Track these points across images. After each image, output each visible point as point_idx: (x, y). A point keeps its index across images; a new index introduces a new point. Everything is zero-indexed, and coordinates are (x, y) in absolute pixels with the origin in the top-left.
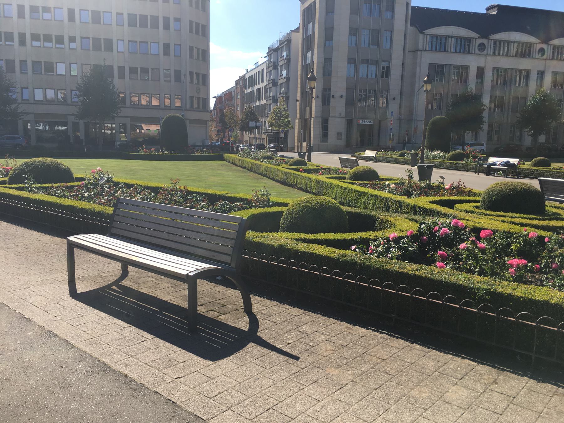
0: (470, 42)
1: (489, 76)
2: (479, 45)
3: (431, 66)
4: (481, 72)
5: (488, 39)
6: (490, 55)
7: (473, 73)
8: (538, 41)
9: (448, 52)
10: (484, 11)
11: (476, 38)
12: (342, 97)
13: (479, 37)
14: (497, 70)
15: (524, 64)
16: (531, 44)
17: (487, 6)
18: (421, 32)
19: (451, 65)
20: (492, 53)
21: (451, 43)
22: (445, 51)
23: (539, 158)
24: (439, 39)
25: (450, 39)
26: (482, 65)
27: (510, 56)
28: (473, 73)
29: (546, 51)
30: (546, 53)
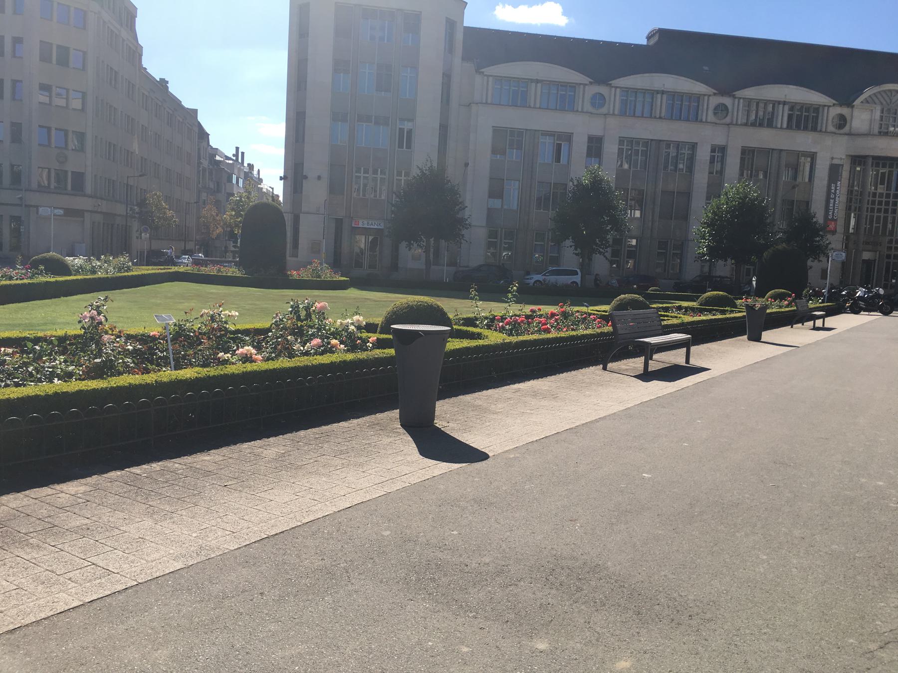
0: (818, 113)
1: (611, 149)
2: (594, 97)
3: (498, 131)
4: (595, 146)
5: (734, 97)
6: (614, 114)
7: (703, 154)
8: (586, 80)
9: (701, 121)
10: (644, 42)
11: (829, 106)
12: (319, 178)
13: (591, 83)
14: (747, 153)
15: (802, 141)
16: (817, 109)
17: (646, 35)
18: (478, 71)
19: (781, 150)
20: (785, 126)
21: (662, 104)
22: (651, 117)
23: (623, 296)
24: (762, 105)
25: (659, 96)
26: (597, 132)
27: (655, 117)
28: (703, 154)
29: (730, 110)
30: (730, 114)
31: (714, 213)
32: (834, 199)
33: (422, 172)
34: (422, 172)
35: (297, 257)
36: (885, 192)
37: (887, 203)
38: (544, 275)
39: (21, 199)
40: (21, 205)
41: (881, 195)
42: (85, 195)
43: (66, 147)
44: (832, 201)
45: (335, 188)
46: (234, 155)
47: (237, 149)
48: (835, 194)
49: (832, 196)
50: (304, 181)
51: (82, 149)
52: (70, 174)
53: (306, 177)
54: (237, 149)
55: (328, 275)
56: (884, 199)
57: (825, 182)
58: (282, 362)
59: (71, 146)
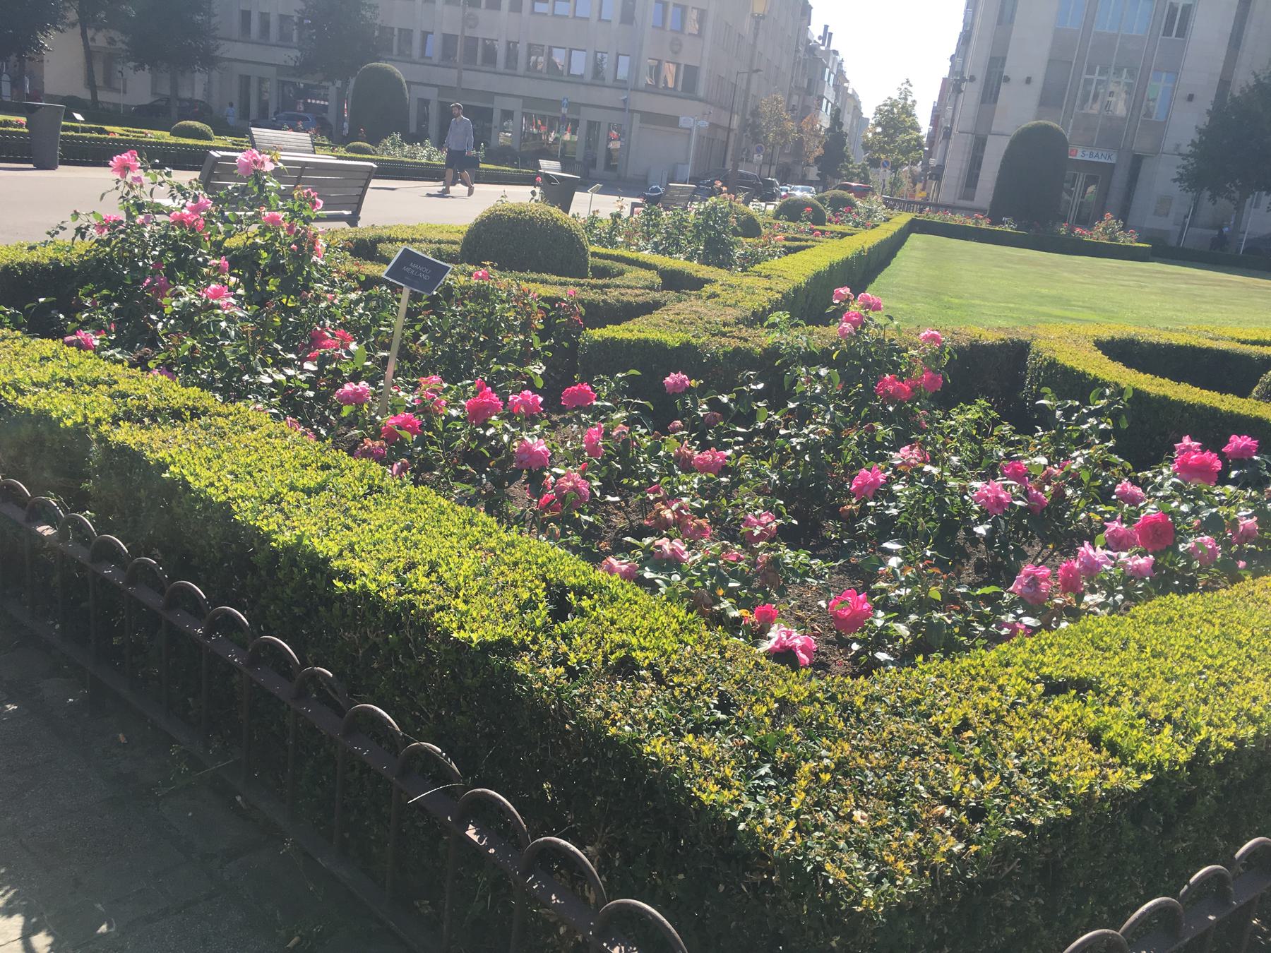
12: (1028, 81)
35: (973, 200)
39: (625, 101)
40: (623, 110)
45: (1050, 98)
46: (820, 38)
47: (826, 27)
52: (682, 68)
53: (1007, 79)
54: (826, 27)
55: (1126, 240)
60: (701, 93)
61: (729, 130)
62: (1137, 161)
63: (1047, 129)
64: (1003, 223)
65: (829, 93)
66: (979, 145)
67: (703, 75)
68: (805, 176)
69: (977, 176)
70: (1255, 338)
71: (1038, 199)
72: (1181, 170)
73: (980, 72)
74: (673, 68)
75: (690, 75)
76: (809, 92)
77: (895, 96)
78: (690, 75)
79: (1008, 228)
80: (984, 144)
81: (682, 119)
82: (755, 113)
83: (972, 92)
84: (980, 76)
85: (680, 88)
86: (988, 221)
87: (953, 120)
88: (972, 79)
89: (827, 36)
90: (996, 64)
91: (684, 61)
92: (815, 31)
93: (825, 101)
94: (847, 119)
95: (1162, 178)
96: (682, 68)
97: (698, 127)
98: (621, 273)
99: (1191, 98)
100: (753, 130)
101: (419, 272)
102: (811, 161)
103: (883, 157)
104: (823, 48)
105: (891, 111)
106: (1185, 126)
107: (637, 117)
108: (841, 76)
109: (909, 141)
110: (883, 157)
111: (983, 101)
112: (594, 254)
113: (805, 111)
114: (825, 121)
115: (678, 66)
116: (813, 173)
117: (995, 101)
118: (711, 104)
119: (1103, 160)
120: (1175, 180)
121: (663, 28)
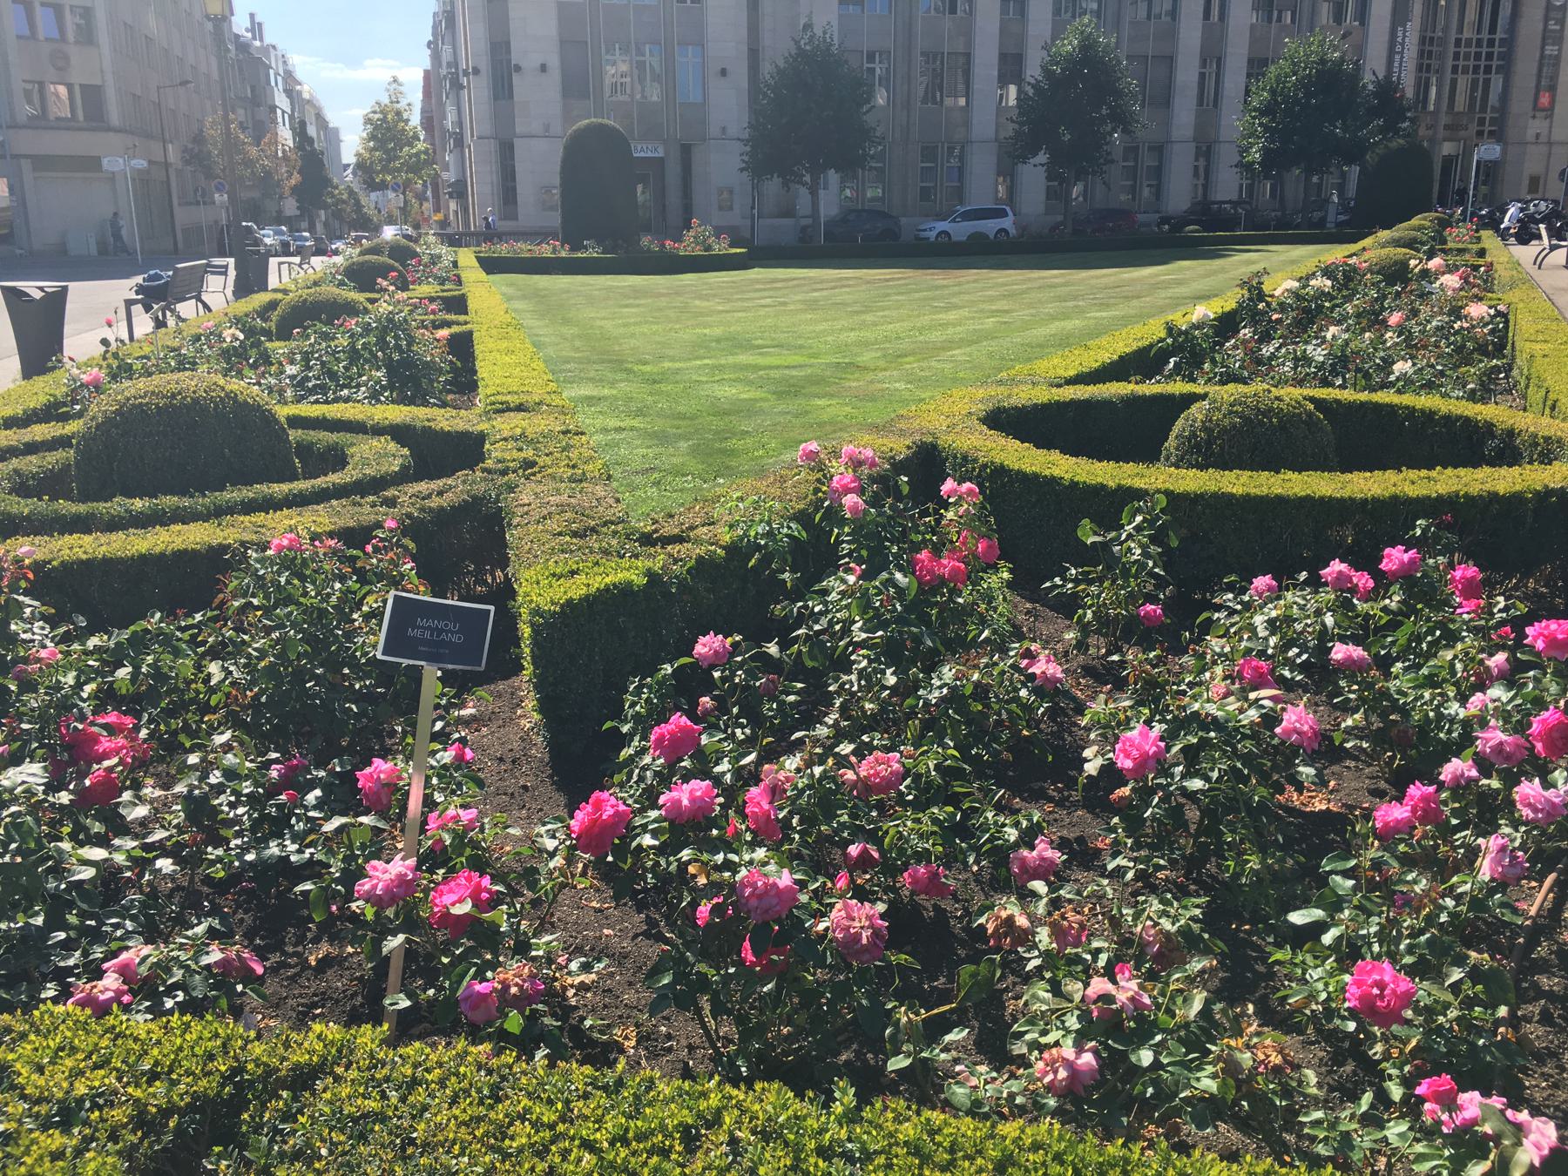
12: (543, 68)
31: (1273, 92)
32: (1402, 53)
33: (799, 48)
34: (799, 48)
36: (1475, 37)
37: (1478, 56)
38: (954, 221)
41: (1469, 43)
42: (109, 129)
43: (63, 39)
44: (1397, 57)
45: (578, 83)
46: (247, 30)
47: (252, 16)
48: (1402, 44)
49: (1398, 48)
50: (516, 78)
51: (87, 36)
52: (77, 90)
53: (518, 68)
54: (252, 16)
55: (721, 247)
56: (1473, 50)
57: (1388, 25)
58: (58, 384)
59: (71, 36)
60: (114, 116)
61: (167, 165)
62: (686, 151)
63: (602, 128)
64: (586, 248)
65: (282, 101)
66: (506, 151)
67: (111, 95)
68: (280, 212)
69: (514, 189)
70: (1072, 373)
71: (614, 214)
72: (746, 158)
73: (477, 60)
74: (62, 90)
75: (92, 96)
76: (258, 100)
77: (386, 101)
78: (92, 96)
79: (593, 253)
80: (511, 147)
81: (105, 162)
82: (199, 139)
83: (477, 92)
84: (484, 65)
85: (81, 118)
86: (567, 247)
87: (460, 124)
88: (476, 71)
89: (256, 28)
90: (500, 49)
91: (77, 79)
92: (240, 24)
93: (279, 112)
94: (312, 131)
95: (722, 166)
96: (77, 90)
97: (132, 169)
98: (337, 459)
99: (724, 72)
100: (196, 156)
101: (440, 631)
102: (287, 192)
103: (389, 178)
104: (257, 43)
105: (384, 120)
106: (729, 108)
107: (26, 165)
108: (289, 76)
109: (417, 155)
110: (389, 178)
111: (496, 98)
112: (296, 422)
113: (262, 128)
114: (286, 135)
115: (70, 87)
116: (290, 207)
117: (511, 96)
118: (132, 133)
119: (650, 154)
120: (742, 170)
121: (33, 35)
